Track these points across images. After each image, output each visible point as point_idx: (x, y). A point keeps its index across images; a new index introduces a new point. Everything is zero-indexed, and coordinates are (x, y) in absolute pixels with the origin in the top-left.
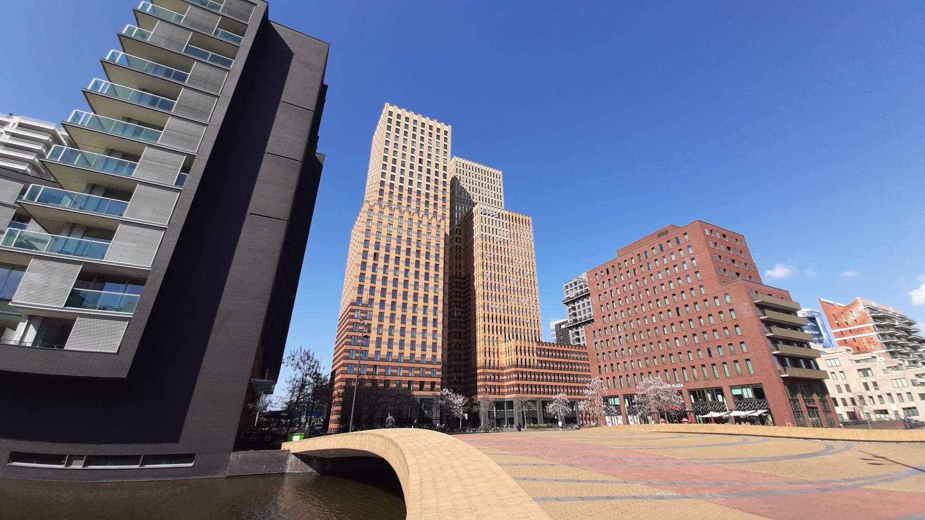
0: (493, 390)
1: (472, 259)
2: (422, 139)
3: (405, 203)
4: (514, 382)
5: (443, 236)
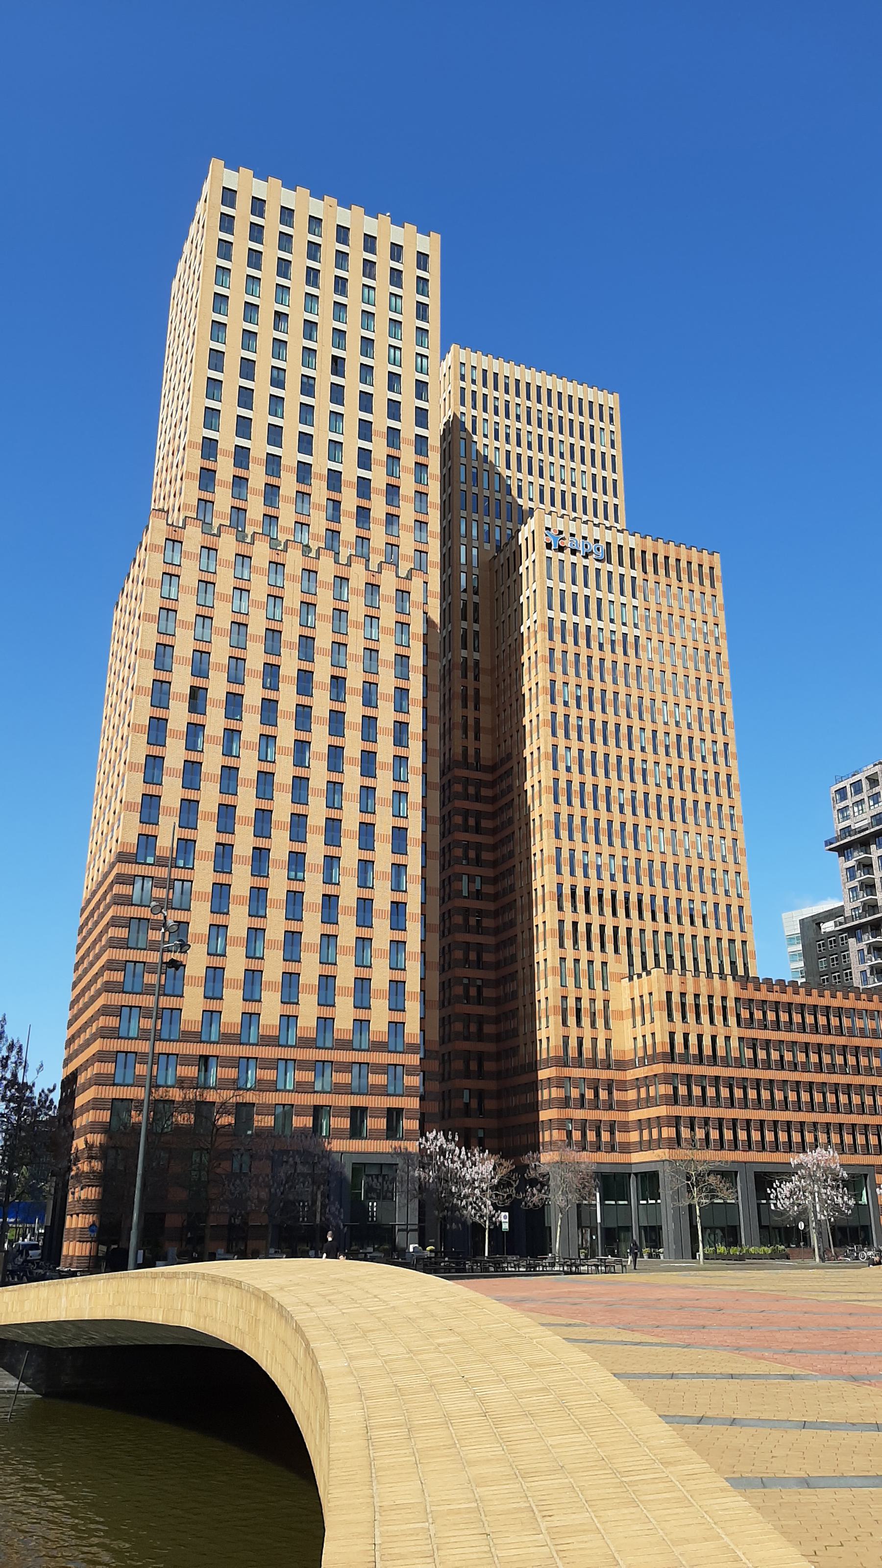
0: (591, 1136)
1: (517, 704)
2: (341, 285)
3: (287, 514)
4: (662, 1111)
5: (417, 627)
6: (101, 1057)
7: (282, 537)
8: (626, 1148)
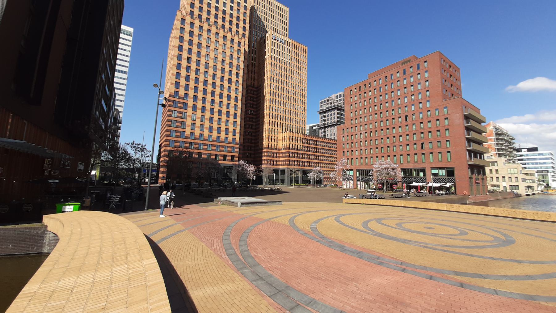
0: (272, 163)
1: (263, 74)
4: (287, 158)
5: (242, 51)
6: (166, 141)
7: (211, 24)
8: (279, 165)
